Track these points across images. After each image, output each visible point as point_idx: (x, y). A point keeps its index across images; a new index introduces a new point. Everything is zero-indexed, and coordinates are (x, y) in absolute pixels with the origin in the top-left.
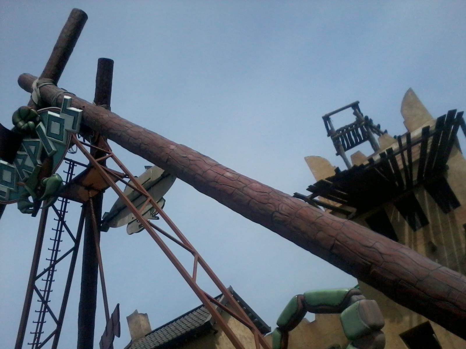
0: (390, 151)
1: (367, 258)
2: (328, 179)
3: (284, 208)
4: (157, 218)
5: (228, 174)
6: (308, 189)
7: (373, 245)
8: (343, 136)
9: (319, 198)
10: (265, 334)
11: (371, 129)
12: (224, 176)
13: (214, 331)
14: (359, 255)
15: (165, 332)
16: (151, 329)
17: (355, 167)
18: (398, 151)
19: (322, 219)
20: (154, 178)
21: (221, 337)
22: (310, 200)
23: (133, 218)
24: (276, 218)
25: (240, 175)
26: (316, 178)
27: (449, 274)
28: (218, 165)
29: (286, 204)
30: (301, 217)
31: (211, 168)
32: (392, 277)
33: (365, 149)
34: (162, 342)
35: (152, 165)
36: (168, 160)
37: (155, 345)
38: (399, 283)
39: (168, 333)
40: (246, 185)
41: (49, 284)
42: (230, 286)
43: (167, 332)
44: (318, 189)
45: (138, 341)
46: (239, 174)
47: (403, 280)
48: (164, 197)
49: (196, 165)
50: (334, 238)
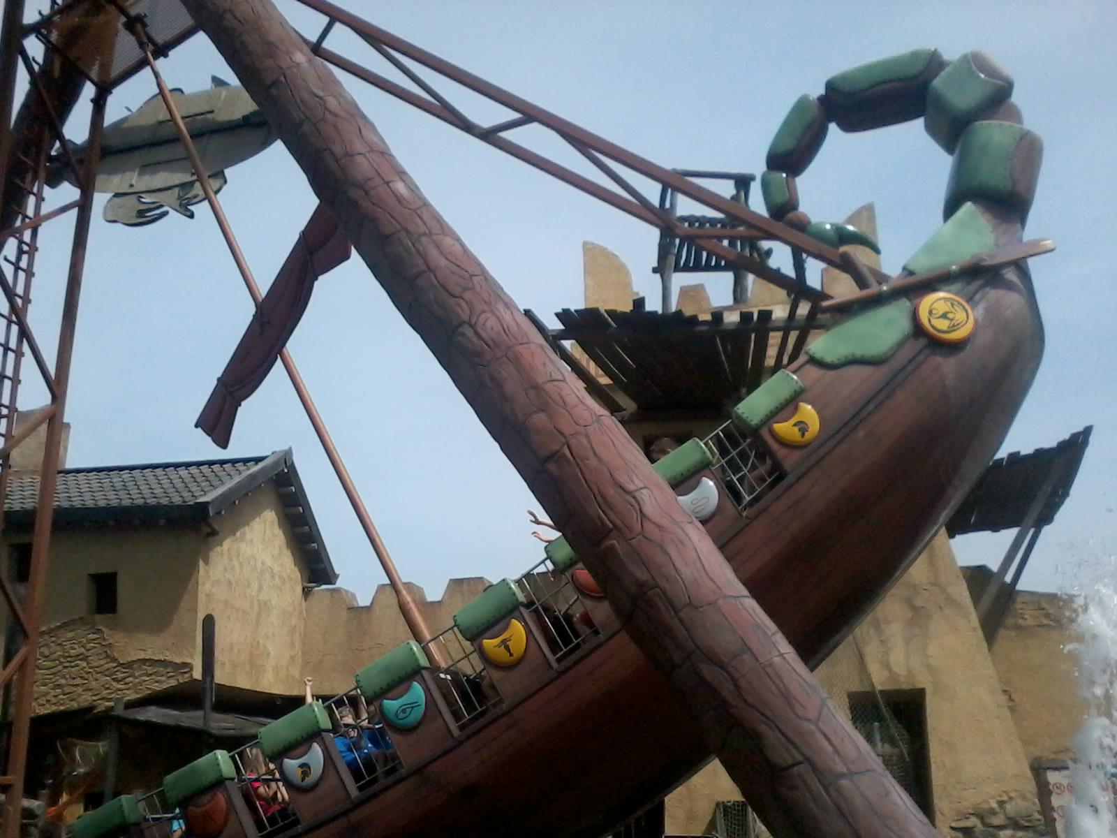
0: (765, 315)
1: (609, 512)
2: (612, 313)
3: (488, 324)
4: (189, 214)
5: (400, 187)
6: (557, 315)
7: (637, 490)
8: (688, 239)
9: (572, 344)
10: (321, 585)
11: (750, 251)
12: (390, 188)
13: (209, 530)
14: (599, 498)
15: (95, 485)
16: (64, 465)
17: (679, 313)
18: (781, 324)
19: (558, 387)
20: (223, 116)
21: (218, 549)
22: (554, 340)
23: (132, 186)
24: (460, 338)
25: (426, 204)
26: (586, 299)
27: (754, 616)
28: (385, 154)
29: (498, 318)
30: (516, 361)
31: (368, 152)
32: (641, 575)
33: (717, 289)
34: (77, 503)
35: (232, 79)
36: (275, 83)
37: (71, 503)
38: (650, 593)
39: (102, 489)
40: (430, 232)
41: (1029, 544)
42: (290, 449)
43: (124, 485)
44: (581, 324)
45: (24, 477)
46: (426, 199)
47: (661, 589)
48: (228, 172)
49: (335, 126)
50: (563, 440)
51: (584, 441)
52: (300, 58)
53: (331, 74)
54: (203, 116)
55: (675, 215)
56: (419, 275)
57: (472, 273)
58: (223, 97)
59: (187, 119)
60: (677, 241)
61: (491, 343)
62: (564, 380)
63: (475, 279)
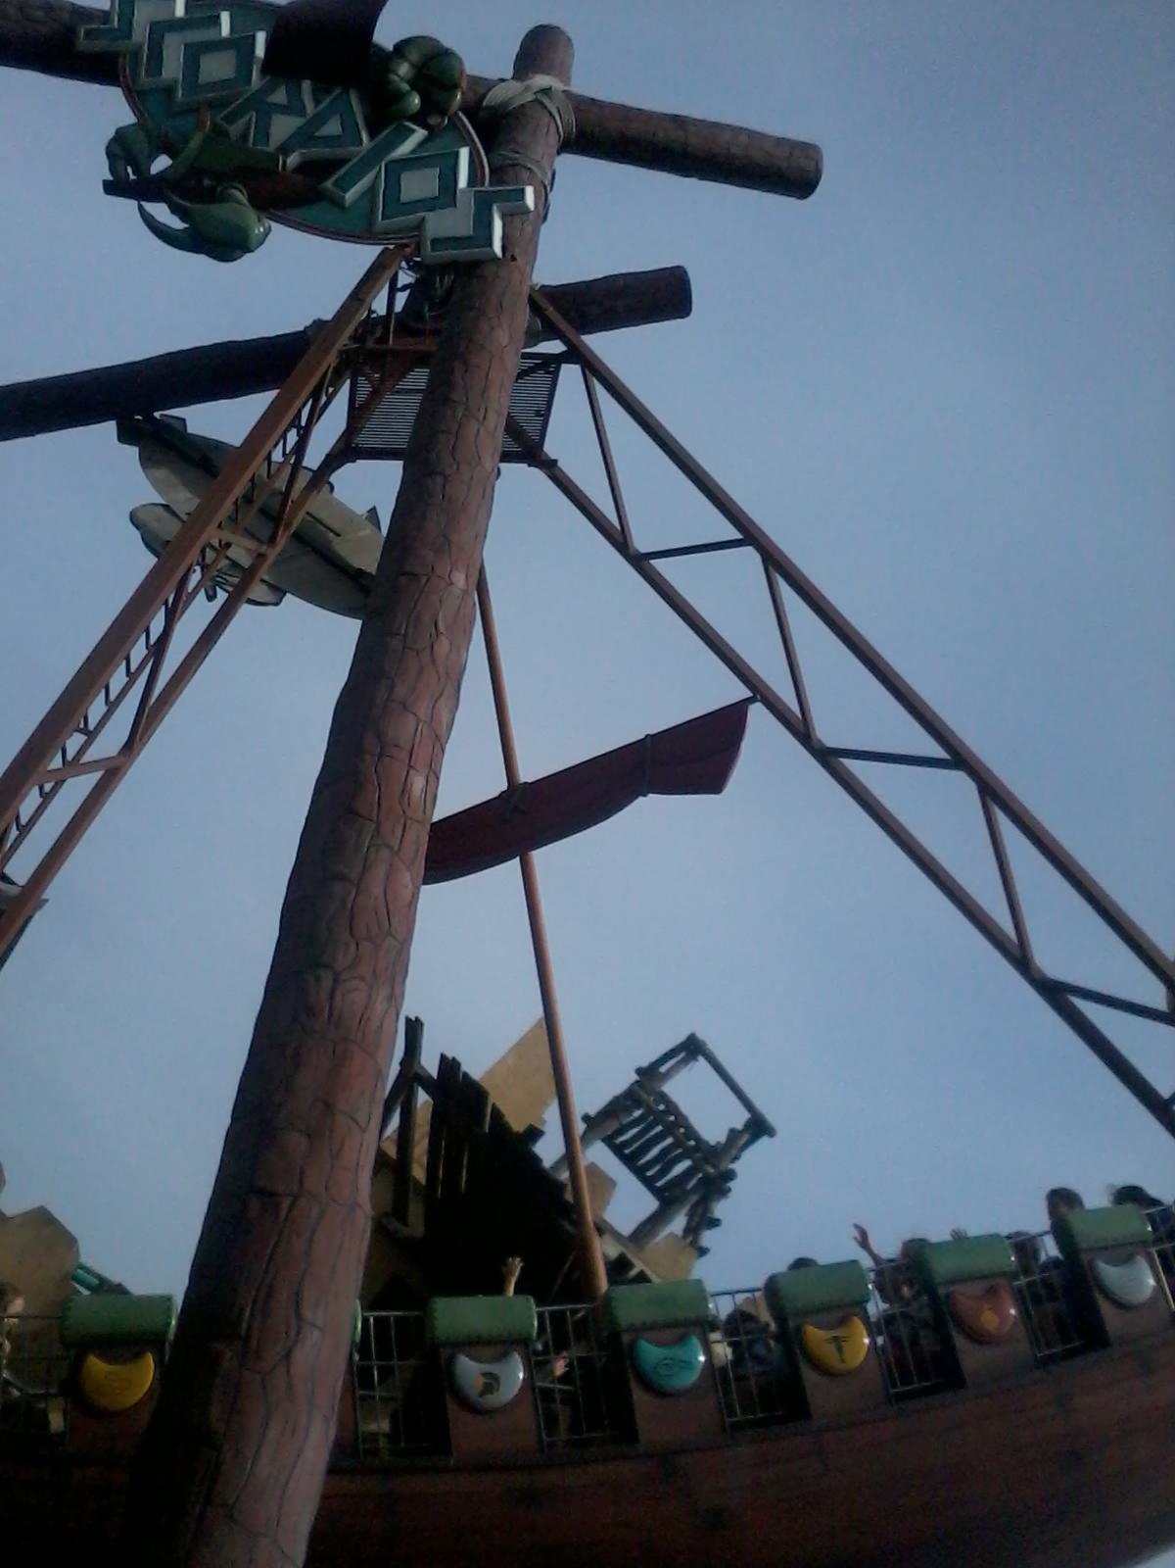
2: (497, 1114)
5: (418, 783)
6: (443, 1058)
9: (426, 1102)
20: (343, 549)
26: (491, 1073)
28: (439, 743)
31: (425, 722)
44: (456, 1091)
49: (421, 670)
51: (315, 1212)
52: (460, 579)
53: (472, 623)
54: (324, 529)
55: (661, 1086)
56: (343, 878)
57: (393, 932)
58: (362, 533)
59: (309, 519)
60: (637, 1113)
61: (336, 1013)
62: (363, 1131)
63: (390, 941)
